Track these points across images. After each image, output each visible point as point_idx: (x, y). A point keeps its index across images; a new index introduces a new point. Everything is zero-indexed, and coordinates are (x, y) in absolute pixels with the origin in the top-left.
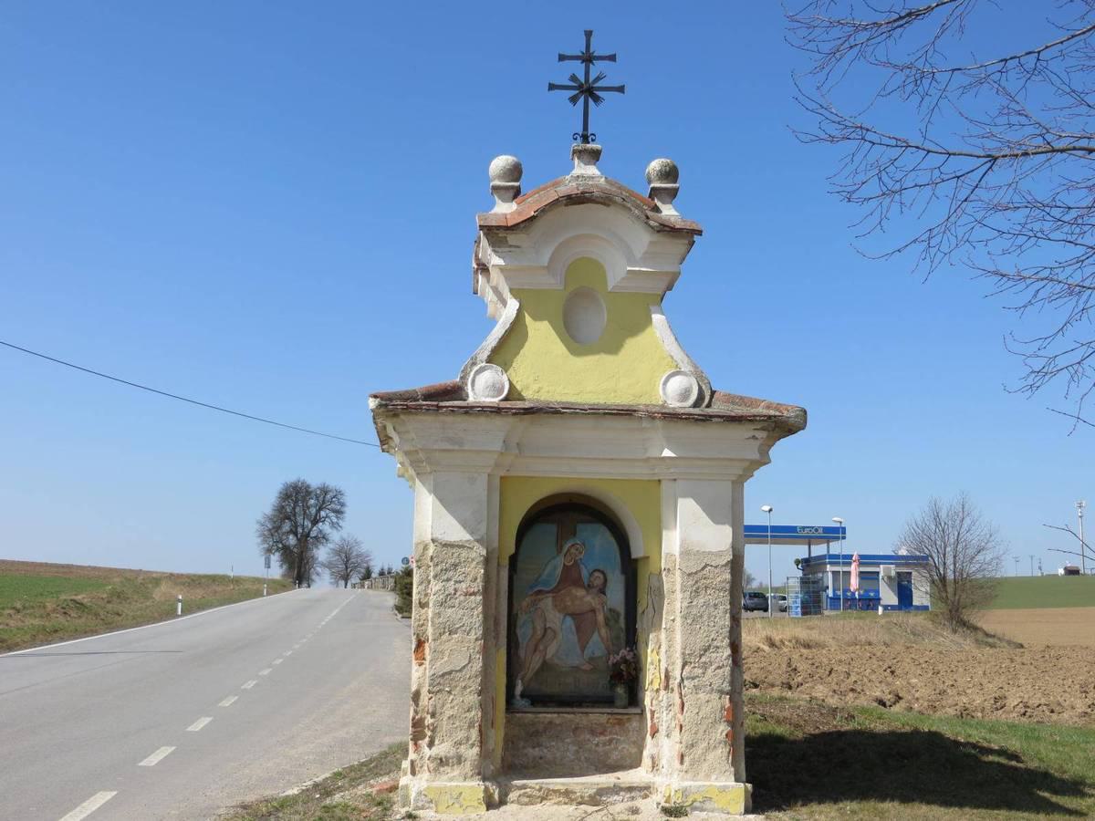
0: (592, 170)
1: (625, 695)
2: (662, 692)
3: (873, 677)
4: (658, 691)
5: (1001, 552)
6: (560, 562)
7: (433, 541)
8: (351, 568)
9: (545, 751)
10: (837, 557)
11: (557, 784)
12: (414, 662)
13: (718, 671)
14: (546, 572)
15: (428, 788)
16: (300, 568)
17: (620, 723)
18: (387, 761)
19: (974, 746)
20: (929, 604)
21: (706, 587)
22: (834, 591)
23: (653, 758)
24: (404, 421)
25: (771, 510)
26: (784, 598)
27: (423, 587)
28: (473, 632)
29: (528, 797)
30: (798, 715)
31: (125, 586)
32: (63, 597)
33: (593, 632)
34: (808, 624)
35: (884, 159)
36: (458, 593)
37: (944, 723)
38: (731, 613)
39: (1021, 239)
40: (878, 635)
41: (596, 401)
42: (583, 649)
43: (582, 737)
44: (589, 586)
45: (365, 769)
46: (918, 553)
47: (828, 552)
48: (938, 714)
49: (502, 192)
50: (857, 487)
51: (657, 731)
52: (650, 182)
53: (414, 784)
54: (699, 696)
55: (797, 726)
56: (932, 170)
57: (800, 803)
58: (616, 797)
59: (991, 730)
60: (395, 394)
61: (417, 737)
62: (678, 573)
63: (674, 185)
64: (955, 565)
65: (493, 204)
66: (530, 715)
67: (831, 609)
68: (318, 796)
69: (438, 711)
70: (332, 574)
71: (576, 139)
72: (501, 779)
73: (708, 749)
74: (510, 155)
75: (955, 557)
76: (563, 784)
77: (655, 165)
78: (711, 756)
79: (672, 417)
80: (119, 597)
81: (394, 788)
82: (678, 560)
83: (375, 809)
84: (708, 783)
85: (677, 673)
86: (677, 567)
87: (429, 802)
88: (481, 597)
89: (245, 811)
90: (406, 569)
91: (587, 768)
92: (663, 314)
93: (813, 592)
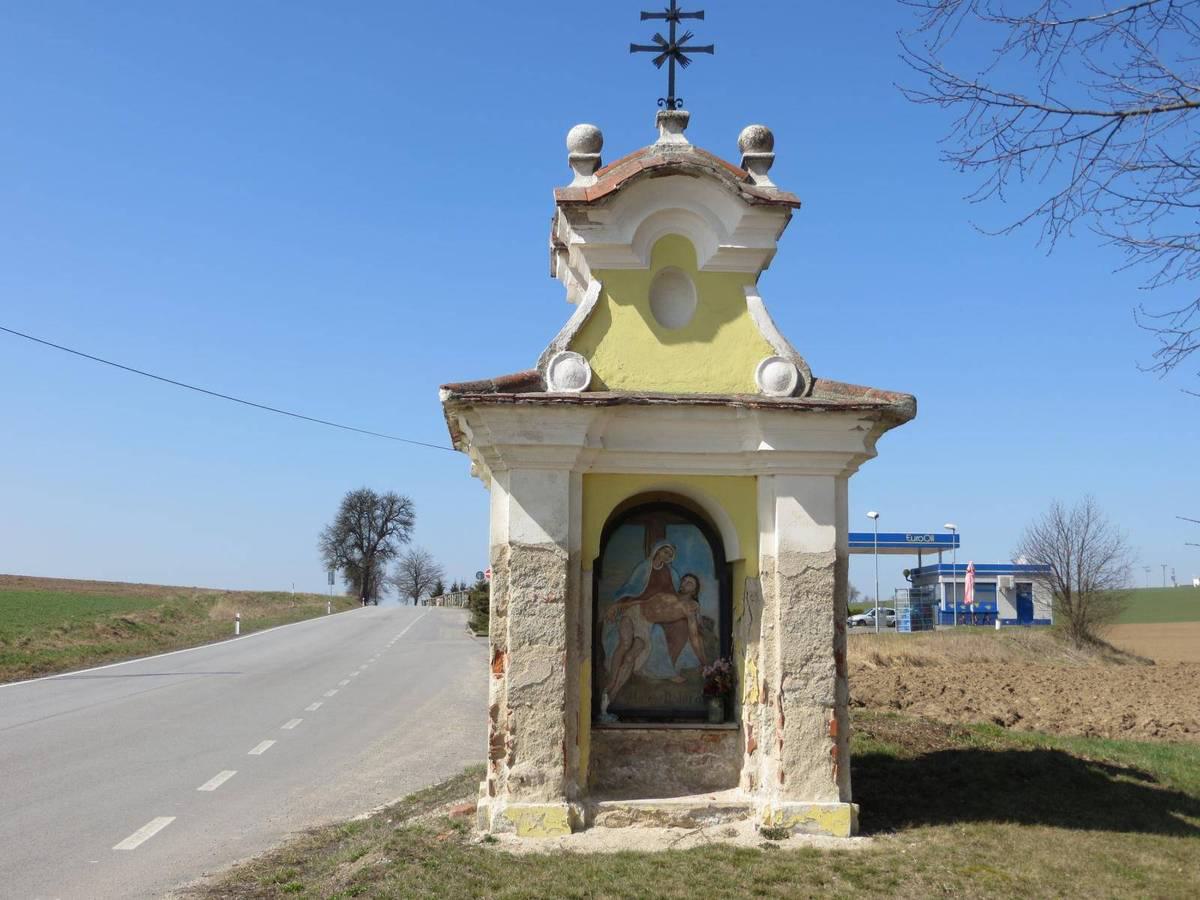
0: (679, 139)
1: (719, 710)
2: (761, 706)
3: (990, 695)
4: (756, 704)
5: (1130, 561)
6: (648, 566)
7: (511, 544)
8: (421, 584)
9: (634, 770)
10: (950, 567)
11: (647, 805)
12: (492, 675)
13: (822, 682)
14: (633, 579)
15: (509, 809)
16: (366, 584)
17: (715, 739)
18: (465, 783)
19: (1101, 765)
20: (1051, 618)
21: (808, 592)
22: (947, 604)
23: (751, 777)
24: (477, 415)
25: (877, 516)
26: (892, 613)
27: (500, 594)
28: (555, 642)
29: (616, 819)
30: (908, 733)
31: (179, 605)
32: (113, 616)
33: (686, 641)
34: (918, 639)
35: (1002, 121)
36: (539, 600)
37: (1068, 740)
38: (834, 619)
39: (1149, 207)
40: (995, 652)
41: (686, 391)
42: (674, 660)
43: (675, 754)
44: (680, 592)
45: (439, 793)
46: (1039, 563)
47: (940, 562)
48: (1062, 733)
49: (582, 164)
50: (970, 488)
51: (756, 748)
52: (742, 150)
53: (493, 806)
54: (800, 709)
55: (908, 744)
56: (1054, 131)
57: (911, 824)
58: (711, 819)
59: (1120, 749)
60: (468, 385)
61: (495, 756)
62: (777, 576)
63: (770, 154)
64: (1079, 575)
65: (571, 178)
66: (617, 731)
67: (943, 624)
68: (390, 821)
69: (519, 726)
70: (401, 590)
71: (661, 105)
72: (587, 800)
73: (810, 768)
74: (590, 123)
75: (1079, 566)
76: (654, 805)
77: (748, 132)
78: (814, 775)
79: (770, 407)
80: (172, 616)
81: (472, 811)
82: (777, 563)
83: (452, 831)
84: (811, 803)
85: (776, 686)
86: (776, 570)
87: (509, 825)
88: (563, 604)
89: (312, 837)
90: (482, 583)
91: (680, 787)
92: (759, 296)
93: (924, 605)
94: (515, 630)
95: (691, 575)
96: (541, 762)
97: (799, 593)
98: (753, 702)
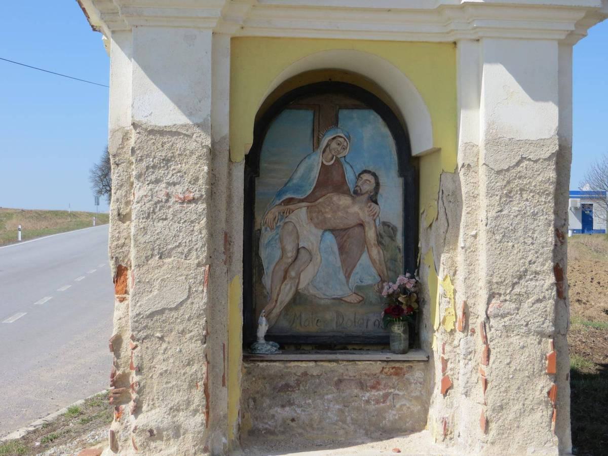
2: (459, 335)
4: (452, 332)
6: (316, 161)
9: (299, 411)
17: (398, 372)
21: (522, 190)
23: (445, 424)
36: (172, 200)
42: (348, 277)
44: (355, 192)
46: (599, 189)
51: (451, 387)
54: (511, 340)
66: (277, 364)
69: (146, 364)
73: (522, 413)
78: (527, 422)
82: (482, 153)
85: (480, 309)
86: (481, 161)
88: (204, 206)
91: (355, 431)
94: (142, 240)
96: (175, 410)
97: (510, 192)
98: (449, 330)
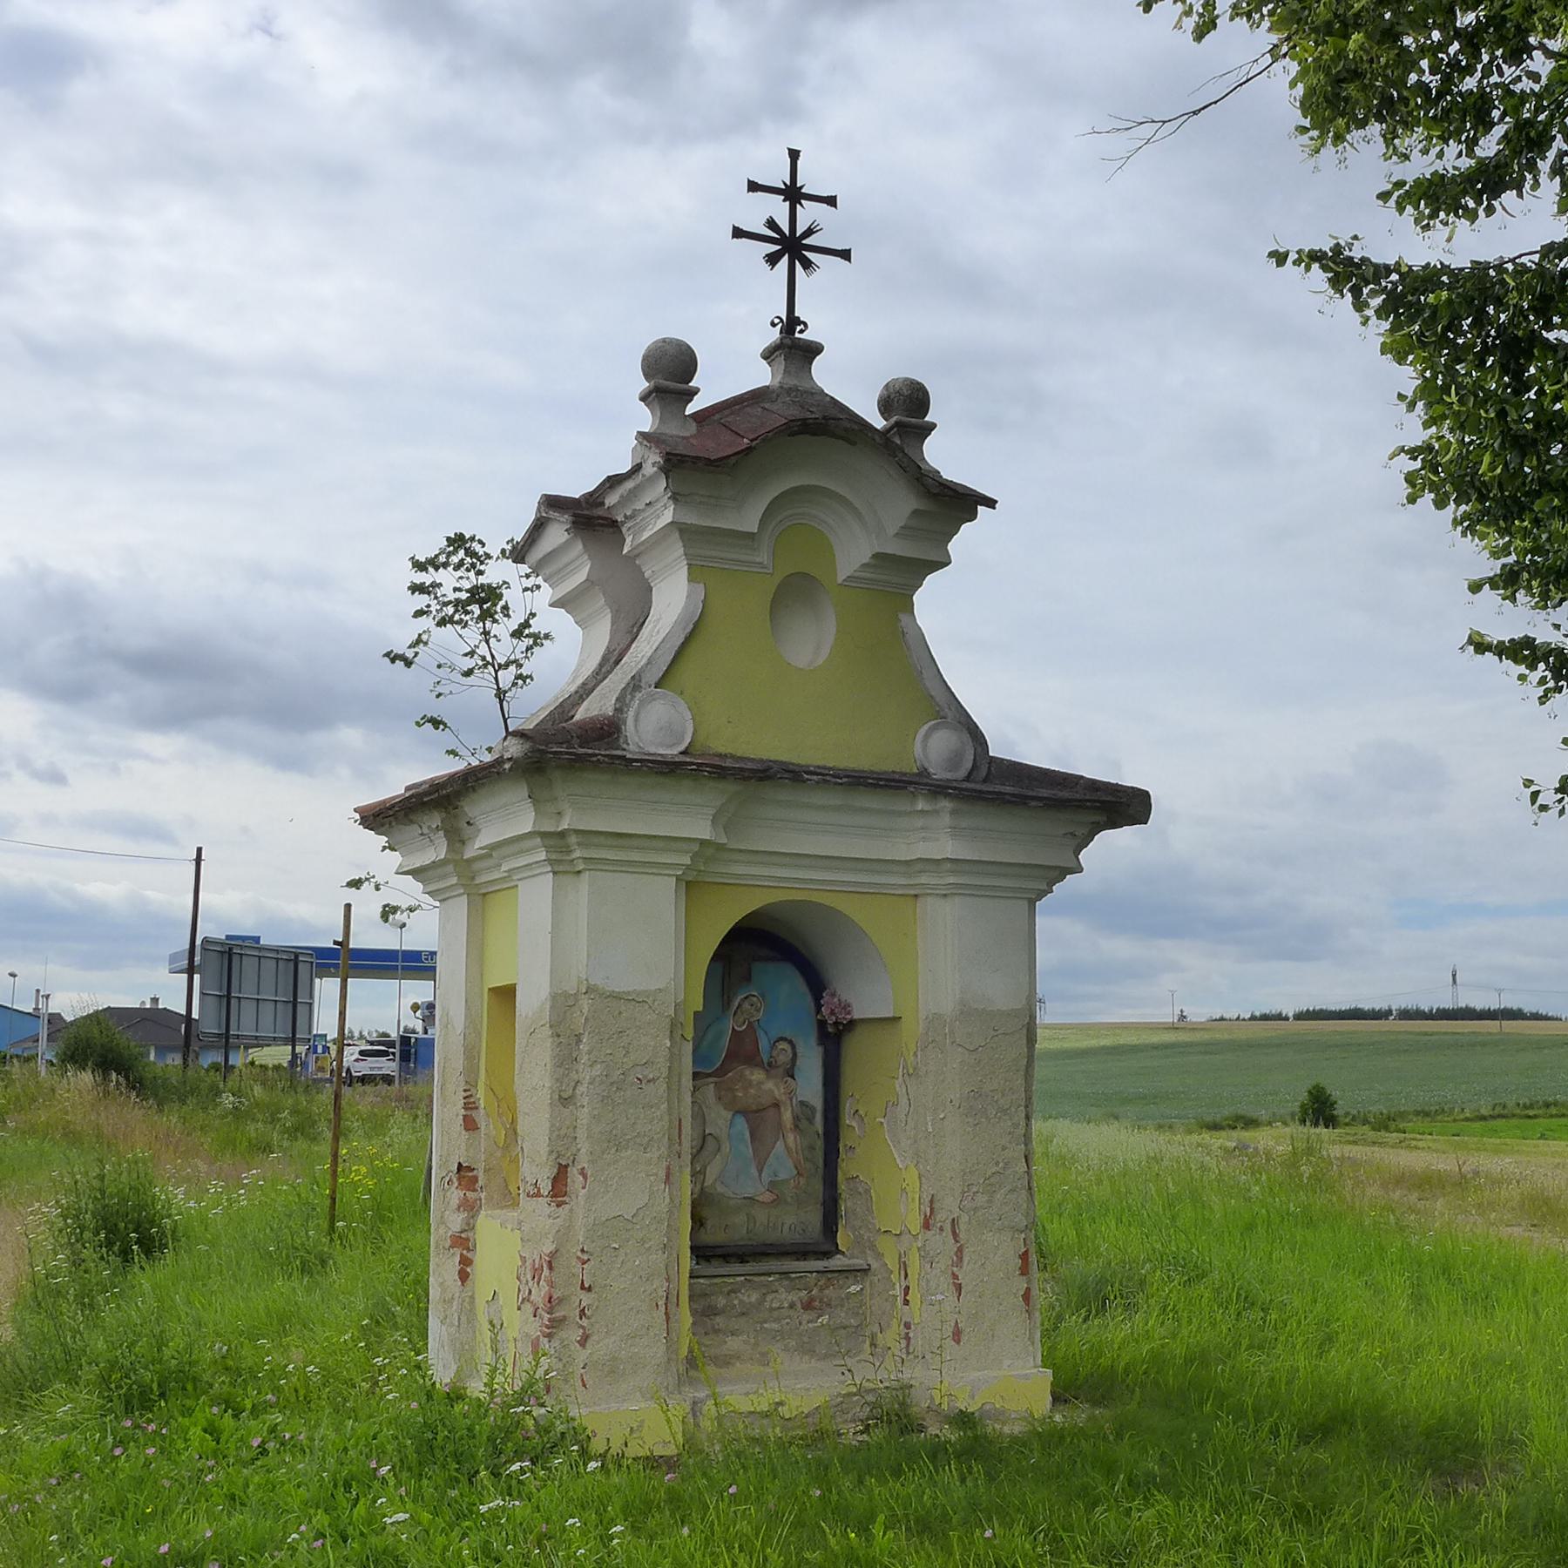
44: (770, 1064)
95: (782, 1039)
